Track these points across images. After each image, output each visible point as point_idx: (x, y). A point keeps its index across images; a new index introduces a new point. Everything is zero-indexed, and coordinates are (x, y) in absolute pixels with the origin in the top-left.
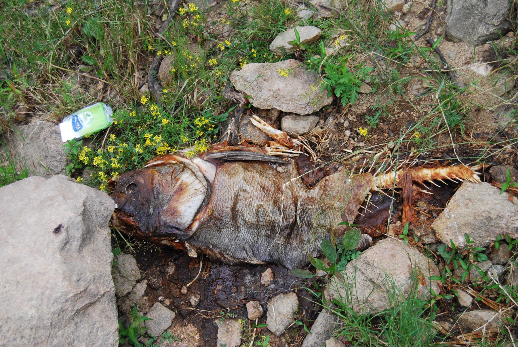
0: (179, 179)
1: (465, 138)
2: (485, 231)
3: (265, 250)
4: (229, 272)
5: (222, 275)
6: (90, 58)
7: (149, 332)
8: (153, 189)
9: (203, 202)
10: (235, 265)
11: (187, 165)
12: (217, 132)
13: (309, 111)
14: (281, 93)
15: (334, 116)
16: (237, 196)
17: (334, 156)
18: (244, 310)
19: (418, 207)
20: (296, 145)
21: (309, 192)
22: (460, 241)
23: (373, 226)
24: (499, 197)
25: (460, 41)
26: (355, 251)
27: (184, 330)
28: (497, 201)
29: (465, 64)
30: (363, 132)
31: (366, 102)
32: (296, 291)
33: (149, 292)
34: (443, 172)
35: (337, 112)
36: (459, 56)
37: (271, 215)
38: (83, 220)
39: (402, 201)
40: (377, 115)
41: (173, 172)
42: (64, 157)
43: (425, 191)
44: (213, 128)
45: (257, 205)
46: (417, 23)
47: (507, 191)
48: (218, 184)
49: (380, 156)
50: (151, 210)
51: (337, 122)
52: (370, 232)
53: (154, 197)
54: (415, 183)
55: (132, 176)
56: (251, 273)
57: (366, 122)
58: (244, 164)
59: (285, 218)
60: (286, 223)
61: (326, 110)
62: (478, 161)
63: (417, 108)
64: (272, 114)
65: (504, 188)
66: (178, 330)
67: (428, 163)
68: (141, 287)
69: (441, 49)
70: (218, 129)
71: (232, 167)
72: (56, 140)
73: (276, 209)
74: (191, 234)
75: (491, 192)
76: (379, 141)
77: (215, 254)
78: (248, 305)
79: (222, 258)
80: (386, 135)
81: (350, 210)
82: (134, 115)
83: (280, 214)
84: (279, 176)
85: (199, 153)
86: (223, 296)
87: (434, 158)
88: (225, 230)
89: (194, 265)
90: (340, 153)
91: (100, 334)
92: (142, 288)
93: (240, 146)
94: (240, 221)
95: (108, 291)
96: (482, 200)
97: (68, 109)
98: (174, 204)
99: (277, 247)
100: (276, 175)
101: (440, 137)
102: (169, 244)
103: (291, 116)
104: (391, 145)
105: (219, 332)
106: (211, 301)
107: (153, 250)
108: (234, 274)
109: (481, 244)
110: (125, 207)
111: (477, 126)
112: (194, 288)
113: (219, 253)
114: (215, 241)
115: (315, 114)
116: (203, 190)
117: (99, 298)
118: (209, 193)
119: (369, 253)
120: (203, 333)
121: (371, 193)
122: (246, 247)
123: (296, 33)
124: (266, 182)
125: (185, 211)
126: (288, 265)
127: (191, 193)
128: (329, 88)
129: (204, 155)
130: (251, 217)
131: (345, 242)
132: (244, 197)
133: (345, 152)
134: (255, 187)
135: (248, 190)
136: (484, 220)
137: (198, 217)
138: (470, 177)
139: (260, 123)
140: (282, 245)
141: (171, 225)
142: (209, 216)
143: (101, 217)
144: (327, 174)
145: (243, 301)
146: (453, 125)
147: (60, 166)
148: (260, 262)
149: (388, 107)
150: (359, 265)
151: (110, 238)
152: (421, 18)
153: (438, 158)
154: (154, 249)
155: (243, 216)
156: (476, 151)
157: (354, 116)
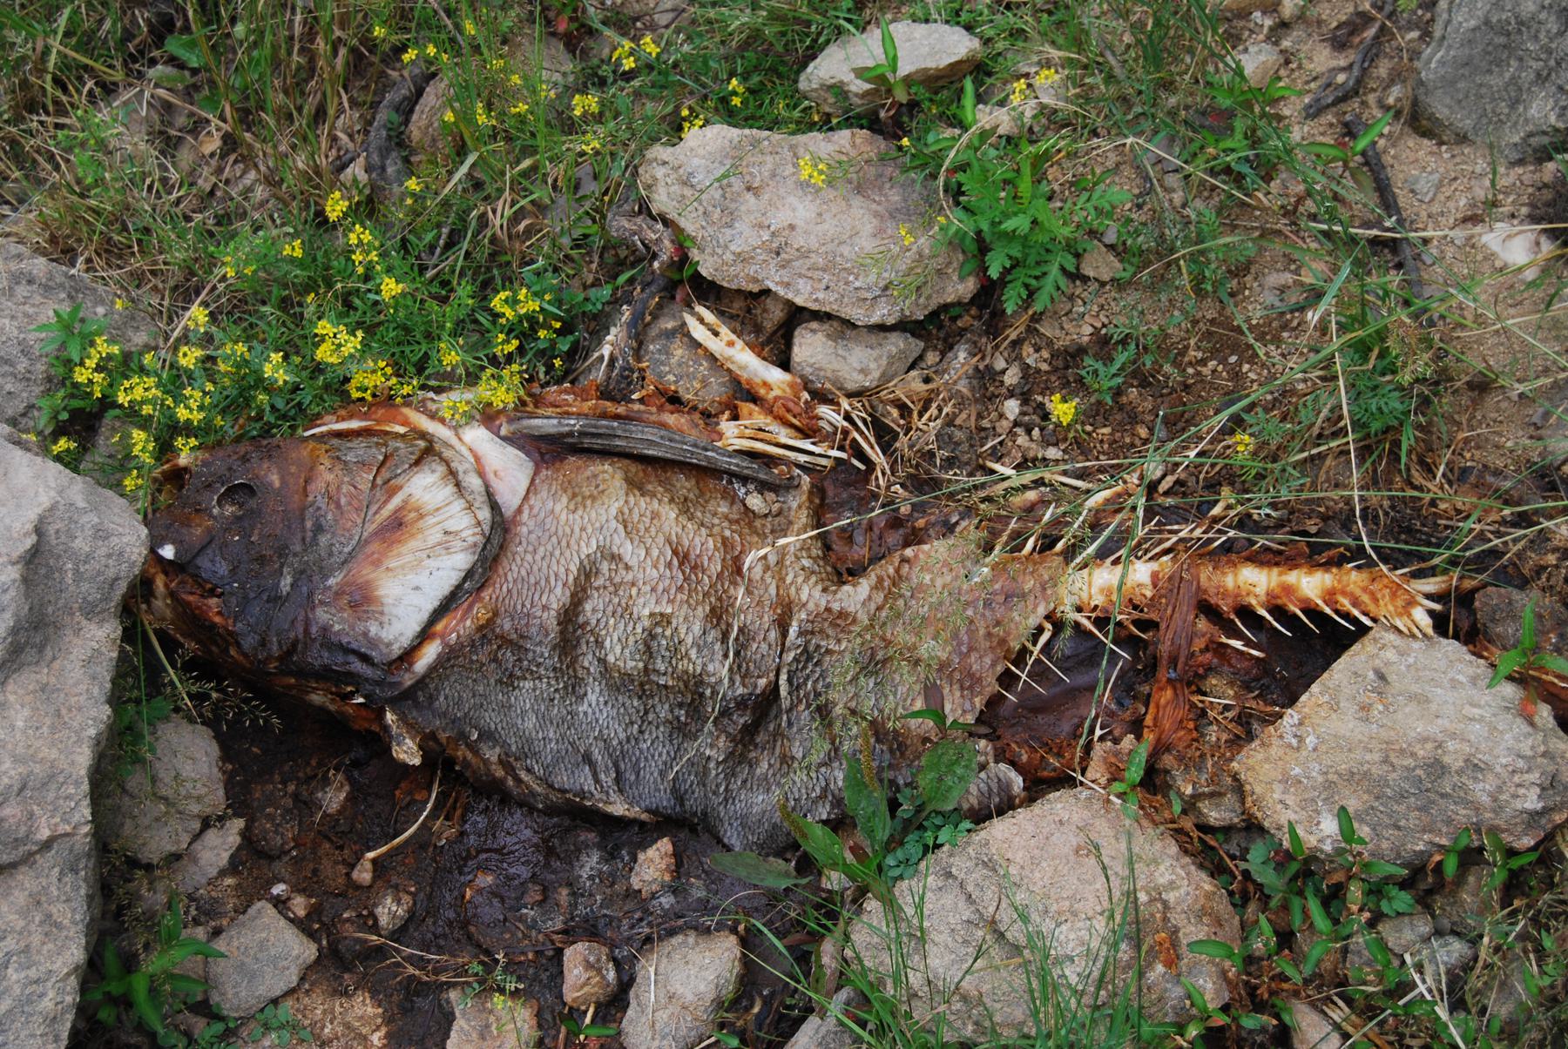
0: (400, 488)
1: (1418, 478)
2: (1419, 809)
3: (662, 774)
4: (528, 833)
5: (504, 840)
6: (192, 45)
7: (215, 998)
8: (303, 510)
9: (465, 579)
10: (551, 811)
11: (437, 447)
12: (565, 348)
13: (882, 313)
14: (798, 241)
15: (975, 343)
16: (587, 573)
17: (949, 481)
18: (554, 970)
19: (1205, 694)
20: (829, 429)
21: (835, 592)
22: (1323, 832)
23: (1039, 739)
24: (1486, 697)
25: (1462, 139)
26: (955, 817)
27: (338, 1009)
28: (1476, 711)
29: (1465, 220)
30: (1063, 410)
31: (1095, 308)
32: (741, 928)
33: (243, 864)
34: (1311, 584)
35: (987, 333)
36: (1447, 191)
37: (693, 653)
38: (25, 580)
39: (1151, 669)
40: (1121, 358)
41: (383, 463)
42: (40, 367)
43: (1237, 644)
44: (556, 331)
45: (652, 615)
46: (1322, 59)
47: (1519, 679)
48: (531, 523)
49: (1107, 501)
50: (286, 583)
51: (981, 367)
52: (1025, 758)
53: (303, 539)
54: (1207, 609)
55: (245, 459)
56: (601, 847)
57: (1080, 380)
58: (634, 468)
59: (740, 668)
60: (740, 691)
61: (954, 319)
62: (1436, 561)
63: (1267, 354)
64: (765, 311)
65: (1504, 669)
66: (317, 1005)
67: (1267, 549)
68: (220, 840)
69: (1387, 160)
70: (570, 338)
71: (588, 473)
72: (27, 307)
73: (713, 634)
74: (408, 680)
75: (1461, 678)
76: (1116, 449)
77: (486, 762)
78: (568, 953)
79: (510, 782)
80: (1143, 432)
81: (971, 676)
82: (298, 253)
83: (726, 656)
84: (750, 525)
85: (488, 410)
86: (492, 911)
87: (1293, 533)
88: (528, 685)
89: (410, 793)
90: (970, 475)
91: (15, 977)
92: (220, 846)
93: (637, 407)
94: (588, 661)
95: (67, 835)
96: (1422, 700)
97: (90, 208)
98: (367, 573)
99: (700, 766)
100: (737, 522)
101: (1328, 462)
102: (332, 708)
103: (826, 326)
104: (1154, 469)
105: (453, 1034)
106: (450, 924)
107: (254, 721)
108: (545, 841)
109: (1398, 855)
110: (199, 561)
111: (1466, 441)
112: (401, 869)
113: (500, 761)
114: (491, 719)
115: (904, 326)
116: (472, 536)
117: (31, 854)
118: (493, 549)
119: (998, 829)
120: (401, 1029)
121: (1048, 626)
122: (597, 755)
123: (887, 42)
124: (697, 541)
125: (399, 600)
126: (732, 837)
127: (430, 543)
128: (972, 247)
129: (503, 419)
130: (627, 651)
131: (925, 780)
132: (610, 579)
133: (993, 472)
134: (655, 553)
135: (627, 558)
136: (1419, 772)
137: (439, 627)
138: (1400, 615)
139: (716, 334)
140: (718, 763)
141: (345, 640)
142: (480, 628)
143: (92, 579)
144: (915, 538)
145: (555, 937)
146: (1376, 426)
147: (25, 395)
148: (635, 812)
149: (1167, 336)
150: (960, 865)
151: (115, 655)
152: (1339, 43)
153: (1305, 533)
154: (257, 718)
155: (599, 644)
156: (1447, 527)
157: (1045, 354)
